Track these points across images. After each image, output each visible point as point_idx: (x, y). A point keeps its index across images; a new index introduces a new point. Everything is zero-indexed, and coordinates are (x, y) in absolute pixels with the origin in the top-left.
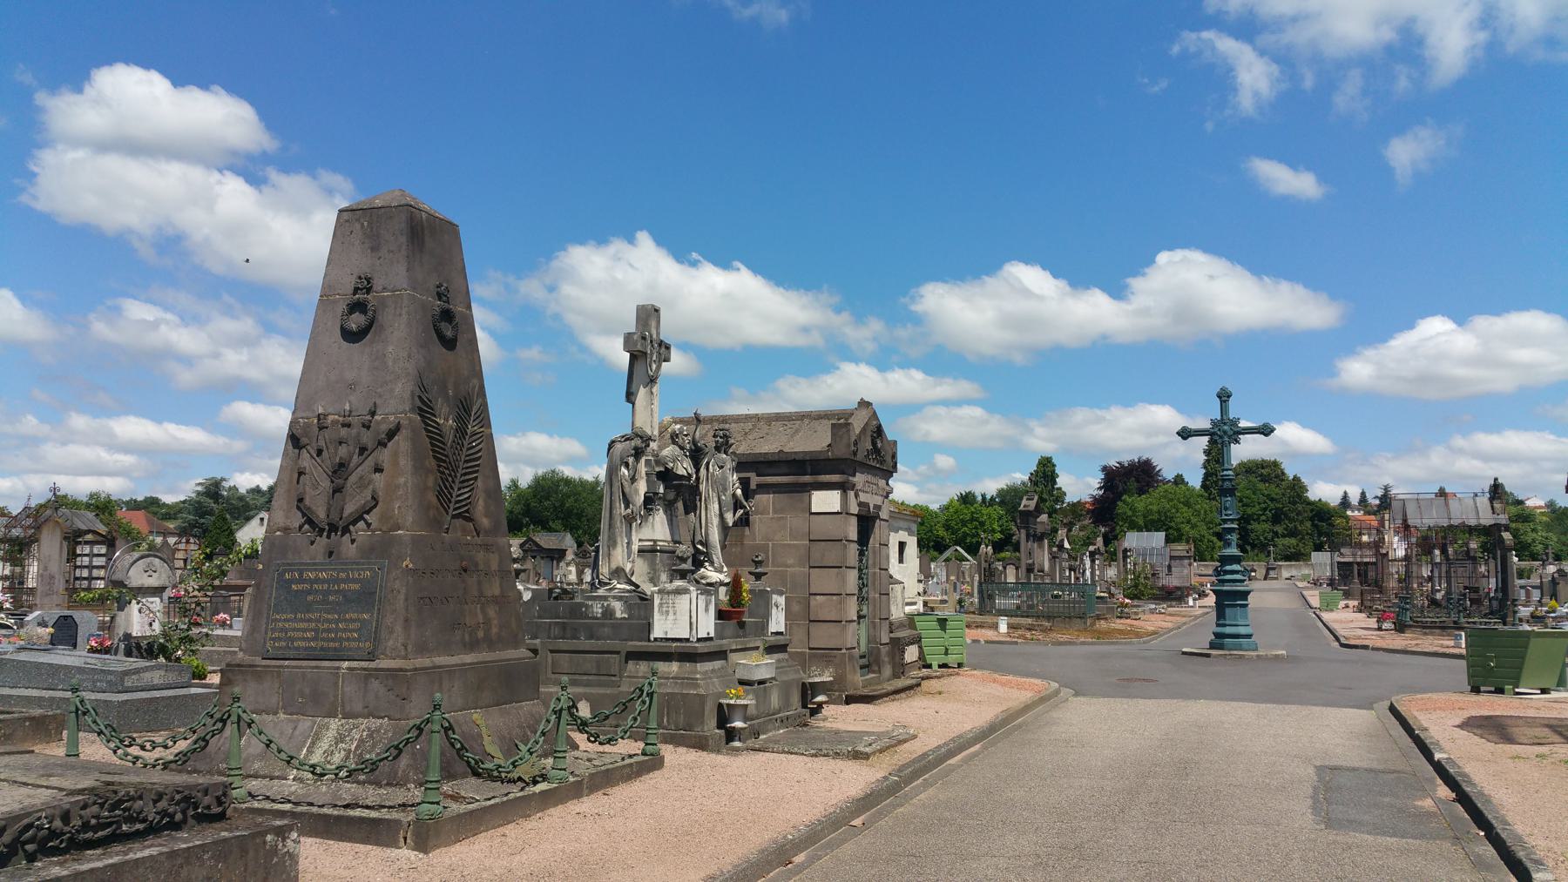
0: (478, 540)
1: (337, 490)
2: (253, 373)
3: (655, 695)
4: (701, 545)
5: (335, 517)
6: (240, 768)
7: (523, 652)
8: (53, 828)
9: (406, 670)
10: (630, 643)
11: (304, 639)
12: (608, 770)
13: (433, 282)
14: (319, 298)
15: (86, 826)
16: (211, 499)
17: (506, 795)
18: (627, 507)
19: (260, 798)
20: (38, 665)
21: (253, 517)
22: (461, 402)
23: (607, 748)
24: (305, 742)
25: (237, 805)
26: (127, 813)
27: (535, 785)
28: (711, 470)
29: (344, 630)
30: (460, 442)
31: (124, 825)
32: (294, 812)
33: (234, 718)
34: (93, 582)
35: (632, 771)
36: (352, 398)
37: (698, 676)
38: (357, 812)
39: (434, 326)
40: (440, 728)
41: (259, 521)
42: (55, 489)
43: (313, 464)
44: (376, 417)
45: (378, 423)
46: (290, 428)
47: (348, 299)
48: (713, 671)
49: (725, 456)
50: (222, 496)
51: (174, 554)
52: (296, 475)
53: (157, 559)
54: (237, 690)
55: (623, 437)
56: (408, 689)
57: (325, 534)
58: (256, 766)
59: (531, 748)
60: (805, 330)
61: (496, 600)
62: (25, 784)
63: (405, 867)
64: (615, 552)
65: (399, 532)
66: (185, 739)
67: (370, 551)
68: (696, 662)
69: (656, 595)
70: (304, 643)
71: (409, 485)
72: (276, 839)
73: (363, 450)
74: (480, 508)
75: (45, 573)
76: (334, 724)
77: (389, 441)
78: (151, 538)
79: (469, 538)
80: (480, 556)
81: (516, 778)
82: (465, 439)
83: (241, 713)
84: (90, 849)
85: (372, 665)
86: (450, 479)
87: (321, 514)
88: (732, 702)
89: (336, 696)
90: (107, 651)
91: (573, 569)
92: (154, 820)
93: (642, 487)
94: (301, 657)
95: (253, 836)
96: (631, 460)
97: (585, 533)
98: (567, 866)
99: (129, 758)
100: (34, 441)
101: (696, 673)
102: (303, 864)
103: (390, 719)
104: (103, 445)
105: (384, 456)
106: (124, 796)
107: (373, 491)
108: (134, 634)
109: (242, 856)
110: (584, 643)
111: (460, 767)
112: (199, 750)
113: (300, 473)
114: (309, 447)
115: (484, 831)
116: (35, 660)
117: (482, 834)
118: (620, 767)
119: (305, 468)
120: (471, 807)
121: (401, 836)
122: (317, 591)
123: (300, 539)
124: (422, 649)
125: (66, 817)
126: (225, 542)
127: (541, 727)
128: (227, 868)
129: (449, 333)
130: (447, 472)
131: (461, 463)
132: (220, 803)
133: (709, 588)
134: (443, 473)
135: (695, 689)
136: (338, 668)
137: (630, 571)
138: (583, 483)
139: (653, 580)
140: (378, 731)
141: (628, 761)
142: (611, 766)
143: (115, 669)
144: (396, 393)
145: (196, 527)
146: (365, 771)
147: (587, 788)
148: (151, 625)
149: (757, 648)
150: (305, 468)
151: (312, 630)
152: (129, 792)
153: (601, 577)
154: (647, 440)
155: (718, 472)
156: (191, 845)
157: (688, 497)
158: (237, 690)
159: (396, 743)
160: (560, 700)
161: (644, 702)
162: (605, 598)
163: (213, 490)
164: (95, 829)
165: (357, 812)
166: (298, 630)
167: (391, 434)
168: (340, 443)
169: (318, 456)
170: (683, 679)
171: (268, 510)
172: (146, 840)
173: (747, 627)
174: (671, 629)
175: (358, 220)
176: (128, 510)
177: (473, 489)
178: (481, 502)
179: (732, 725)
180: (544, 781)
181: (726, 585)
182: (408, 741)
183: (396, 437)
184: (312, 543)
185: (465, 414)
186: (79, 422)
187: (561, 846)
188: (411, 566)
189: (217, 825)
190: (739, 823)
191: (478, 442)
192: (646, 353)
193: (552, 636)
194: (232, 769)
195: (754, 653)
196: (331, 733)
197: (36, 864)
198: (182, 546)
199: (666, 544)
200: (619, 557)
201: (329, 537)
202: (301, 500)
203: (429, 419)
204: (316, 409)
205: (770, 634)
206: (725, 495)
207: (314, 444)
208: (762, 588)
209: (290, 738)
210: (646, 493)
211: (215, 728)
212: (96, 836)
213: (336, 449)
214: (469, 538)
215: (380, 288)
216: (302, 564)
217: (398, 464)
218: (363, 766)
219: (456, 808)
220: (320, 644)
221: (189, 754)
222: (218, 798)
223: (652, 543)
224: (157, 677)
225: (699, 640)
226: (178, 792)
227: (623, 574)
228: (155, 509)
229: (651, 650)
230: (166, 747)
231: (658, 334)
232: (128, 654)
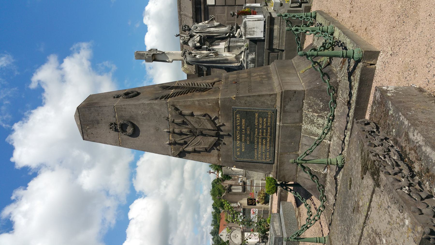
1: (202, 134)
4: (227, 35)
14: (121, 147)
28: (198, 31)
29: (263, 125)
39: (131, 98)
43: (191, 145)
65: (219, 102)
69: (247, 37)
76: (305, 126)
77: (180, 110)
87: (212, 140)
89: (292, 127)
94: (274, 145)
103: (304, 99)
123: (223, 148)
136: (279, 126)
143: (274, 239)
144: (159, 108)
146: (333, 93)
151: (262, 141)
162: (247, 62)
170: (280, 21)
174: (260, 29)
175: (87, 131)
215: (114, 119)
216: (233, 147)
220: (268, 136)
223: (226, 49)
227: (238, 56)
229: (268, 38)
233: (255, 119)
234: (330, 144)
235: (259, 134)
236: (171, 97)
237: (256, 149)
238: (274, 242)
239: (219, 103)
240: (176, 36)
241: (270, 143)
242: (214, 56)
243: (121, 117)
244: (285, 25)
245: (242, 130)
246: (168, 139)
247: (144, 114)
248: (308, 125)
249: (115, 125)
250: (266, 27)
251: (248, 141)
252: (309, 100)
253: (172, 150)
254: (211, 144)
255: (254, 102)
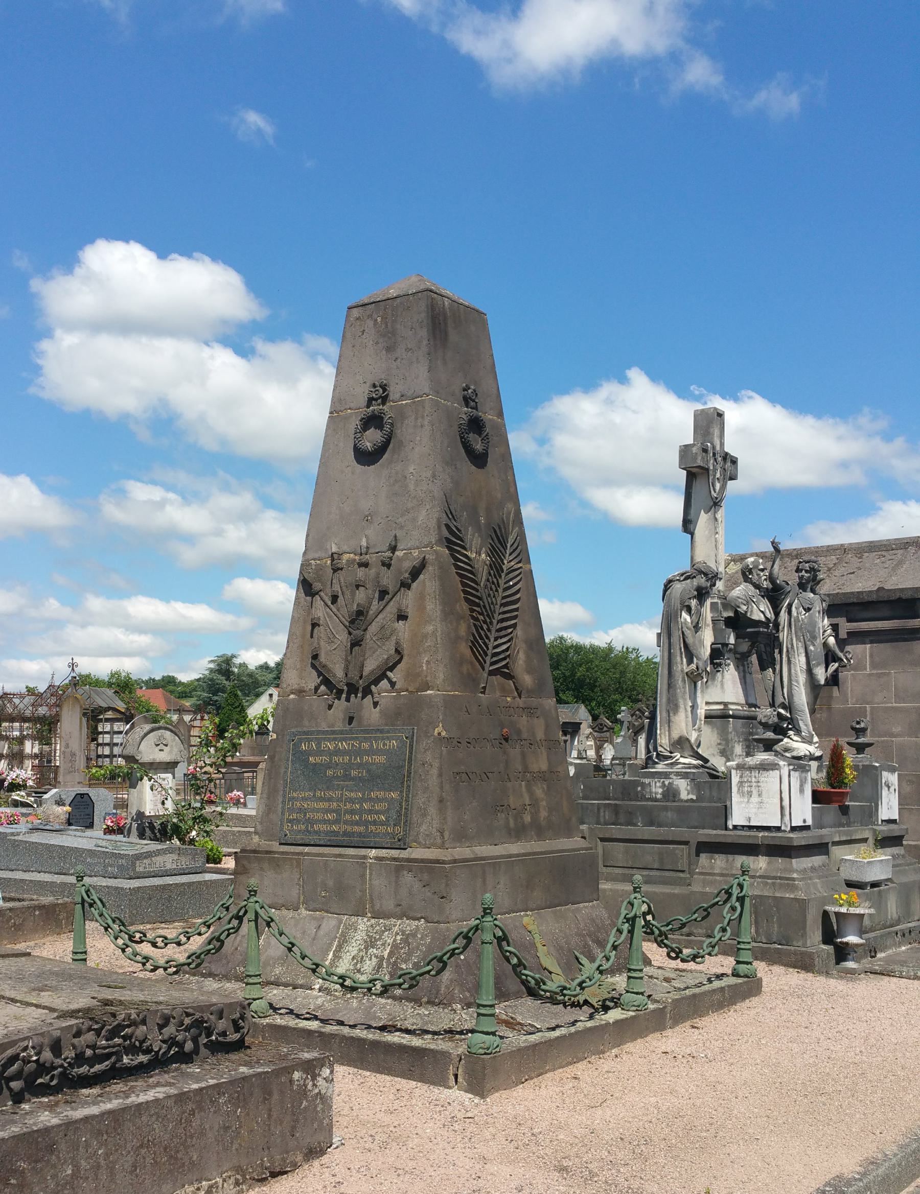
0: (520, 702)
1: (356, 643)
2: (252, 549)
3: (747, 900)
5: (354, 675)
6: (259, 975)
7: (576, 842)
8: (41, 1060)
9: (444, 862)
10: (701, 831)
11: (325, 822)
12: (694, 995)
13: (459, 383)
14: (328, 415)
15: (80, 1059)
16: (223, 676)
17: (574, 1023)
18: (690, 661)
19: (282, 1011)
20: (49, 848)
21: (262, 693)
22: (495, 531)
23: (691, 965)
24: (331, 944)
25: (257, 1020)
26: (128, 1042)
27: (606, 1013)
29: (370, 812)
30: (495, 580)
31: (125, 1057)
32: (321, 1032)
33: (251, 915)
34: (115, 759)
35: (723, 996)
36: (368, 532)
37: (795, 875)
38: (395, 1038)
39: (461, 438)
40: (492, 938)
41: (268, 697)
42: (73, 665)
43: (327, 613)
44: (397, 553)
45: (400, 560)
46: (301, 572)
47: (361, 412)
48: (813, 869)
49: (812, 595)
50: (233, 672)
51: (189, 732)
52: (310, 628)
53: (168, 733)
54: (253, 881)
55: (682, 575)
56: (447, 885)
57: (344, 696)
58: (277, 971)
59: (601, 965)
60: (844, 465)
61: (543, 777)
62: (14, 1001)
63: (460, 1115)
64: (676, 718)
65: (429, 692)
66: (200, 934)
67: (394, 717)
68: (790, 857)
69: (733, 772)
70: (325, 826)
71: (439, 634)
72: (304, 1076)
73: (383, 593)
74: (521, 662)
75: (67, 750)
76: (363, 924)
78: (168, 716)
79: (509, 699)
80: (523, 721)
81: (581, 1002)
82: (500, 577)
83: (259, 910)
84: (86, 1088)
85: (404, 854)
86: (485, 627)
87: (338, 672)
88: (843, 910)
89: (363, 891)
90: (120, 831)
91: (591, 743)
92: (160, 1049)
93: (708, 637)
94: (322, 842)
95: (277, 1073)
96: (694, 603)
97: (599, 704)
98: (667, 1130)
99: (139, 958)
100: (57, 624)
101: (792, 871)
102: (338, 1103)
103: (427, 921)
104: (119, 627)
105: (408, 600)
106: (124, 1020)
107: (397, 643)
108: (147, 814)
109: (265, 1099)
110: (642, 830)
111: (513, 984)
112: (213, 951)
113: (314, 625)
114: (322, 594)
115: (550, 1070)
116: (47, 842)
117: (547, 1075)
118: (709, 992)
119: (319, 619)
120: (533, 1038)
121: (451, 1072)
122: (337, 765)
123: (316, 703)
124: (461, 836)
125: (56, 1047)
126: (237, 719)
127: (612, 939)
128: (248, 1114)
129: (479, 447)
130: (481, 617)
131: (497, 607)
132: (237, 1029)
133: (799, 763)
134: (477, 619)
135: (792, 891)
136: (365, 857)
137: (696, 739)
138: (594, 650)
139: (726, 753)
140: (414, 935)
141: (717, 984)
142: (697, 990)
143: (126, 852)
144: (420, 522)
145: (210, 704)
147: (671, 1018)
148: (163, 803)
149: (865, 840)
150: (319, 619)
151: (334, 811)
152: (130, 1015)
153: (660, 749)
154: (713, 577)
155: (803, 616)
156: (203, 1085)
157: (763, 650)
158: (253, 881)
159: (439, 954)
160: (632, 905)
161: (733, 909)
162: (666, 775)
163: (225, 667)
164: (92, 1062)
165: (395, 1038)
166: (318, 811)
167: (416, 573)
168: (358, 587)
169: (332, 603)
170: (775, 878)
171: (277, 686)
172: (151, 1077)
173: (851, 812)
175: (370, 316)
176: (147, 688)
177: (512, 638)
178: (522, 656)
179: (845, 940)
180: (616, 1006)
181: (819, 759)
182: (453, 953)
183: (421, 577)
184: (330, 707)
185: (499, 546)
186: (95, 604)
187: (653, 1100)
188: (444, 734)
189: (234, 1056)
190: (888, 1080)
191: (515, 581)
192: (707, 470)
193: (602, 820)
194: (250, 976)
195: (862, 847)
196: (360, 936)
197: (23, 1106)
198: (197, 723)
199: (740, 708)
200: (682, 724)
201: (348, 700)
202: (315, 657)
203: (458, 552)
204: (328, 547)
205: (880, 823)
206: (814, 645)
207: (329, 591)
208: (867, 763)
209: (314, 939)
210: (713, 644)
211: (231, 926)
212: (92, 1070)
213: (353, 594)
214: (509, 699)
215: (398, 396)
216: (319, 732)
217: (425, 608)
218: (401, 980)
219: (517, 1040)
221: (202, 956)
222: (235, 1022)
223: (721, 707)
224: (169, 862)
225: (794, 829)
226: (188, 1015)
227: (688, 745)
228: (171, 688)
229: (729, 840)
230: (179, 944)
231: (722, 444)
232: (142, 835)
233: (384, 790)
234: (312, 989)
235: (349, 803)
236: (452, 555)
237: (314, 796)
238: (117, 852)
239: (426, 691)
240: (773, 543)
241: (327, 833)
242: (686, 671)
243: (401, 413)
244: (762, 890)
245: (359, 755)
246: (345, 548)
247: (408, 480)
248: (364, 934)
249: (381, 397)
250: (761, 834)
251: (334, 773)
252: (422, 934)
253: (318, 562)
254: (329, 671)
255: (427, 788)
